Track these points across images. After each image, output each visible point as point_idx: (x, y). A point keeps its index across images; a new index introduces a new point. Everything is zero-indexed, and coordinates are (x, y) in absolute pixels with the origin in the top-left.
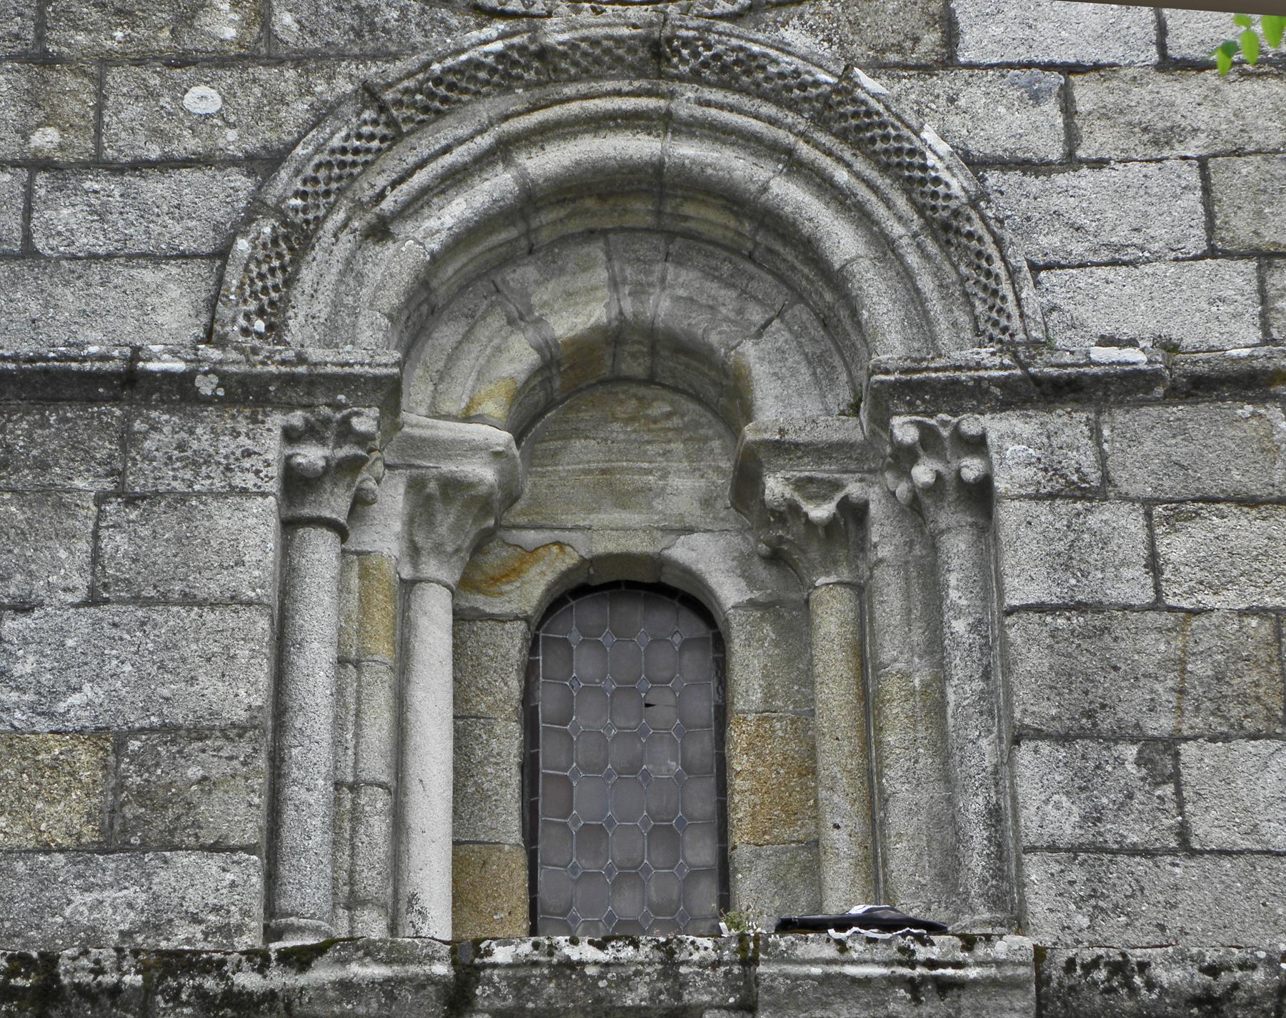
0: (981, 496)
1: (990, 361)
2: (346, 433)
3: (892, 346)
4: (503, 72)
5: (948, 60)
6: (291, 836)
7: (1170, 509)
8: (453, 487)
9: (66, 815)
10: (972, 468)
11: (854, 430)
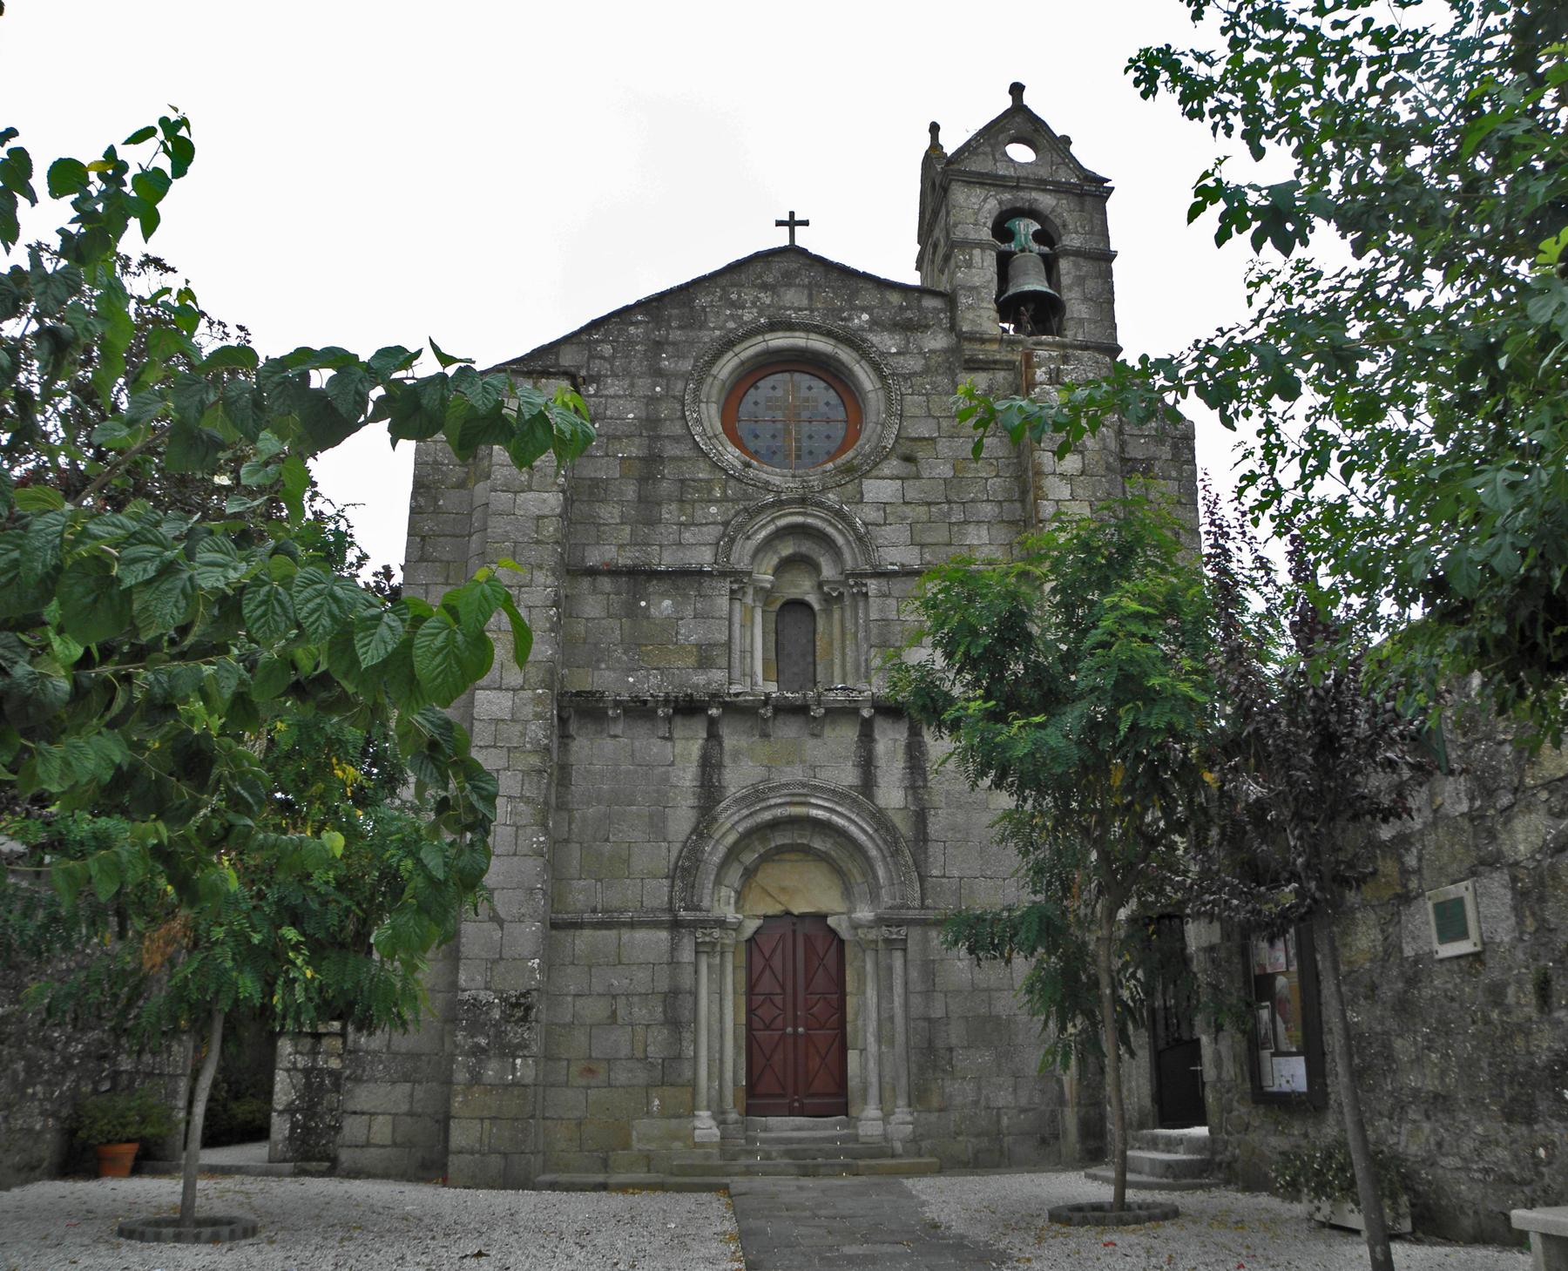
4: (773, 505)
5: (861, 501)
8: (762, 588)
9: (691, 661)
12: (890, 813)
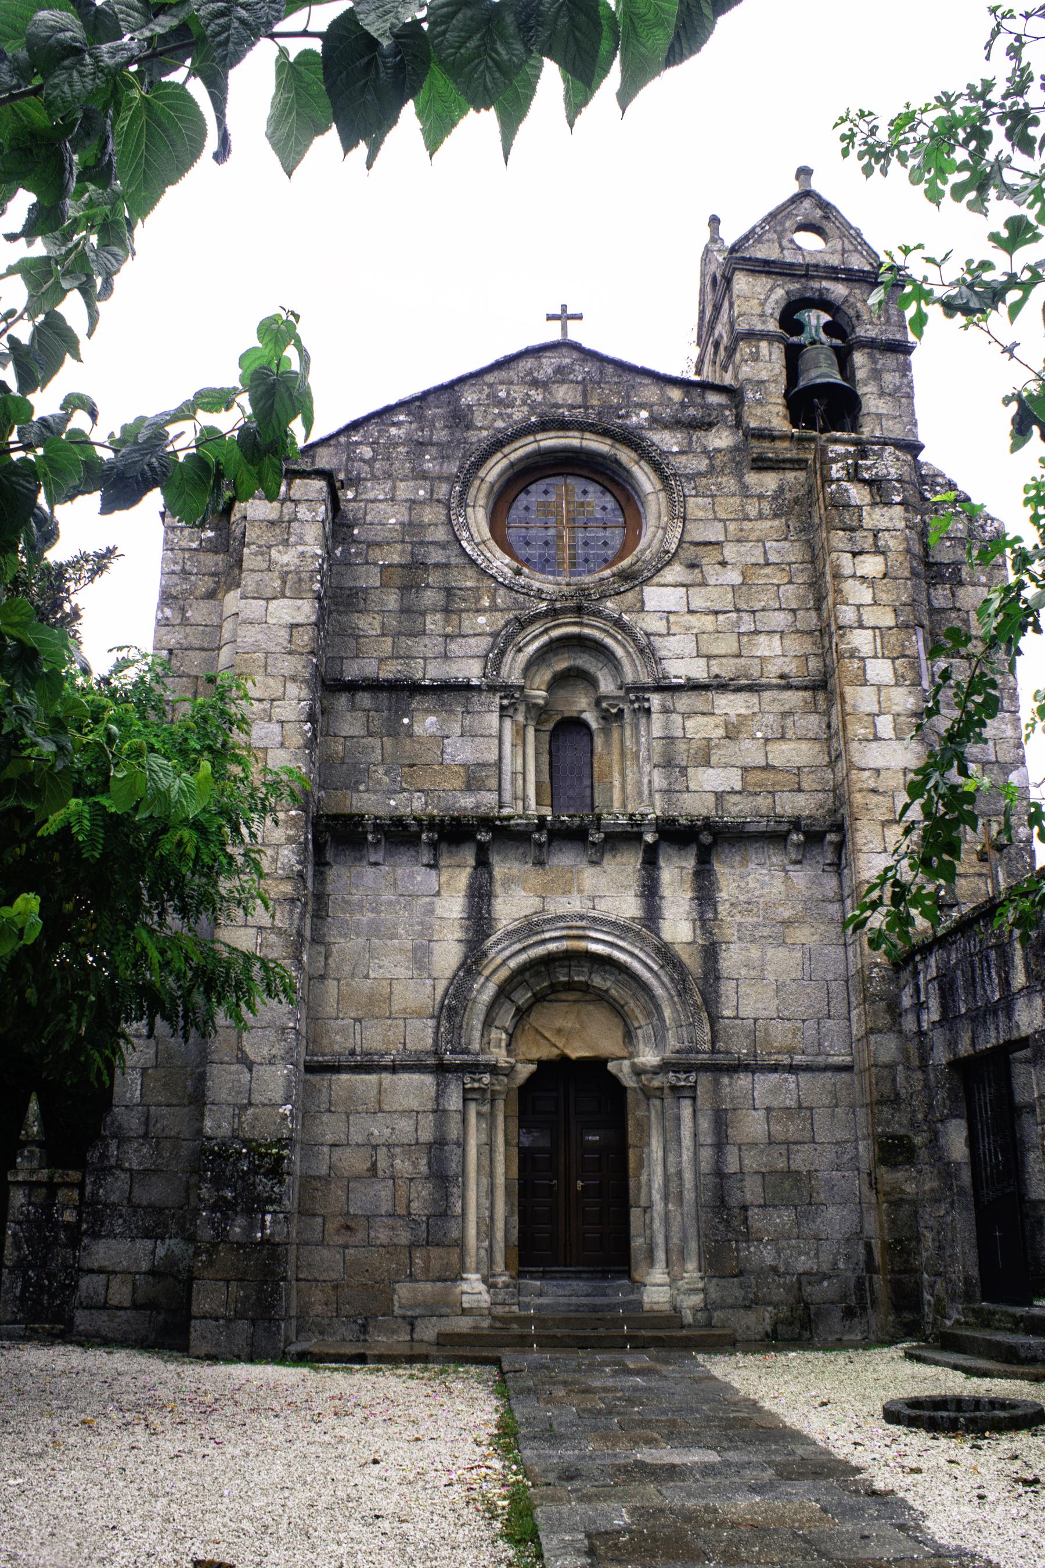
0: (648, 711)
1: (649, 681)
2: (513, 697)
3: (629, 678)
5: (642, 610)
6: (504, 786)
7: (687, 715)
8: (535, 705)
9: (458, 783)
10: (646, 705)
11: (621, 693)
12: (677, 947)
